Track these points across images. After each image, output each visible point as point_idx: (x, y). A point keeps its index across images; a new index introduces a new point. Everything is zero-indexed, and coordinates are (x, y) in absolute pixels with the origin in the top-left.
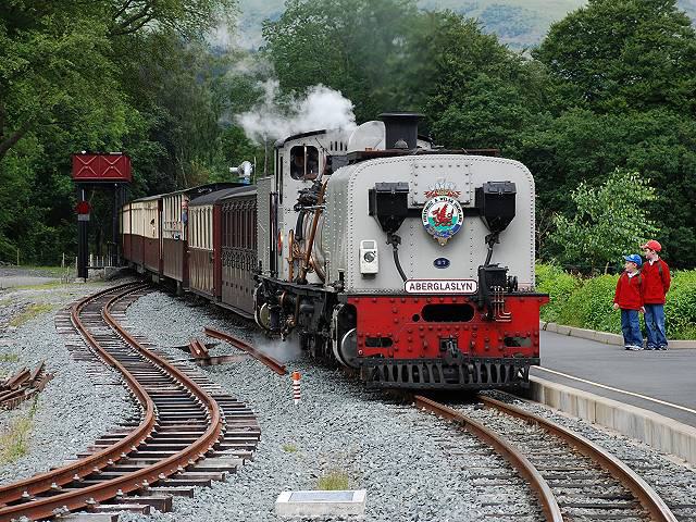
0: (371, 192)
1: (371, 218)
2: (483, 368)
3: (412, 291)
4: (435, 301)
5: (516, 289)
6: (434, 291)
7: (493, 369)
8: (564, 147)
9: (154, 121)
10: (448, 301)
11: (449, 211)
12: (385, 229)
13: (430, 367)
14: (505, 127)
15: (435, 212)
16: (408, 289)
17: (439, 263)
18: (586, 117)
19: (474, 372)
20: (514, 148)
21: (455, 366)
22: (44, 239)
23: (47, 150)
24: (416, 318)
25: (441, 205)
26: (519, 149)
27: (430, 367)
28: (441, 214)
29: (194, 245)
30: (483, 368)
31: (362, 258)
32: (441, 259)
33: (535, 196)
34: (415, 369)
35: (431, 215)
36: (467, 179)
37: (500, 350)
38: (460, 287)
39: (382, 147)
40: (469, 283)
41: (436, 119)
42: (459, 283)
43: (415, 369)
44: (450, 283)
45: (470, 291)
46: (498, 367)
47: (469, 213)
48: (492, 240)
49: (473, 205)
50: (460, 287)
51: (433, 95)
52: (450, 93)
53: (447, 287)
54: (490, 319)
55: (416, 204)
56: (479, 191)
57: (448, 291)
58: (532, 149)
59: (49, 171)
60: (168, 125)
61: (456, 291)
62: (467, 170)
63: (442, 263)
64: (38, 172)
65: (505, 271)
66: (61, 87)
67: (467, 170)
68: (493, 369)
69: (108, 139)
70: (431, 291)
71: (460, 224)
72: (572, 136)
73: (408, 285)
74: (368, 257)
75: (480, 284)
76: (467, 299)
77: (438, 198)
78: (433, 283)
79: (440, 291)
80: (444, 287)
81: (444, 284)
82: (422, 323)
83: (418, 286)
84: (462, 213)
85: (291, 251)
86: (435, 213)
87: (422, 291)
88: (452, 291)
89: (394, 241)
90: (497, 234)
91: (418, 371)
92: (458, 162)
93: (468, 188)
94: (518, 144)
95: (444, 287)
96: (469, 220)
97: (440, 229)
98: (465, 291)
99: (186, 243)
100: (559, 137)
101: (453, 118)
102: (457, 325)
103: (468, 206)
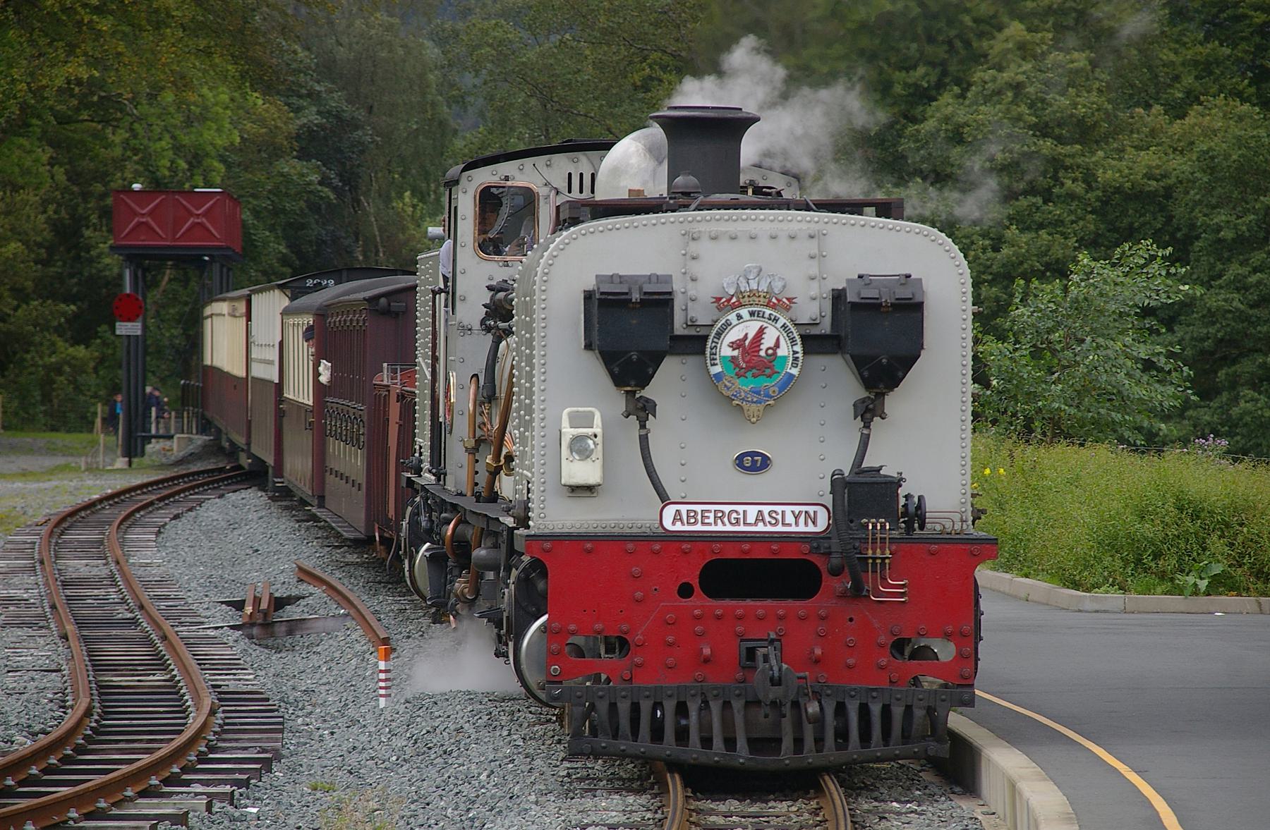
0: (588, 296)
1: (589, 354)
2: (841, 709)
3: (678, 527)
4: (731, 553)
5: (922, 527)
6: (729, 528)
7: (864, 710)
8: (1186, 183)
9: (311, 116)
10: (760, 553)
11: (768, 342)
12: (618, 381)
13: (715, 707)
14: (1060, 140)
15: (735, 345)
16: (668, 524)
17: (748, 461)
18: (1241, 119)
19: (819, 721)
20: (1079, 188)
21: (775, 705)
22: (59, 371)
23: (73, 177)
24: (685, 591)
25: (752, 328)
26: (1090, 188)
27: (715, 707)
28: (750, 348)
29: (289, 394)
30: (841, 709)
31: (565, 451)
32: (753, 454)
33: (970, 308)
34: (682, 710)
35: (726, 351)
36: (814, 271)
37: (882, 668)
38: (790, 519)
39: (658, 188)
40: (811, 509)
41: (914, 120)
42: (788, 509)
43: (682, 710)
44: (766, 509)
45: (811, 528)
46: (876, 709)
47: (813, 343)
48: (868, 412)
49: (826, 327)
50: (790, 519)
51: (907, 70)
52: (943, 64)
53: (760, 518)
54: (857, 592)
55: (692, 324)
56: (838, 297)
57: (760, 527)
58: (1118, 190)
59: (79, 221)
60: (342, 123)
61: (780, 528)
62: (813, 247)
63: (754, 463)
64: (56, 226)
65: (898, 483)
66: (71, 49)
67: (813, 247)
68: (864, 710)
69: (196, 159)
70: (720, 528)
71: (795, 371)
72: (1209, 162)
73: (670, 512)
74: (579, 447)
75: (833, 515)
76: (805, 547)
77: (744, 312)
78: (727, 509)
79: (742, 528)
80: (751, 519)
81: (752, 511)
82: (699, 602)
83: (719, 517)
84: (798, 348)
85: (474, 426)
86: (734, 345)
87: (699, 527)
88: (769, 529)
89: (643, 410)
90: (881, 396)
91: (686, 716)
92: (767, 226)
93: (814, 289)
94: (1089, 179)
95: (751, 519)
96: (820, 361)
97: (746, 385)
98: (802, 528)
99: (279, 387)
100: (1180, 165)
101: (947, 119)
102: (782, 606)
103: (815, 331)
